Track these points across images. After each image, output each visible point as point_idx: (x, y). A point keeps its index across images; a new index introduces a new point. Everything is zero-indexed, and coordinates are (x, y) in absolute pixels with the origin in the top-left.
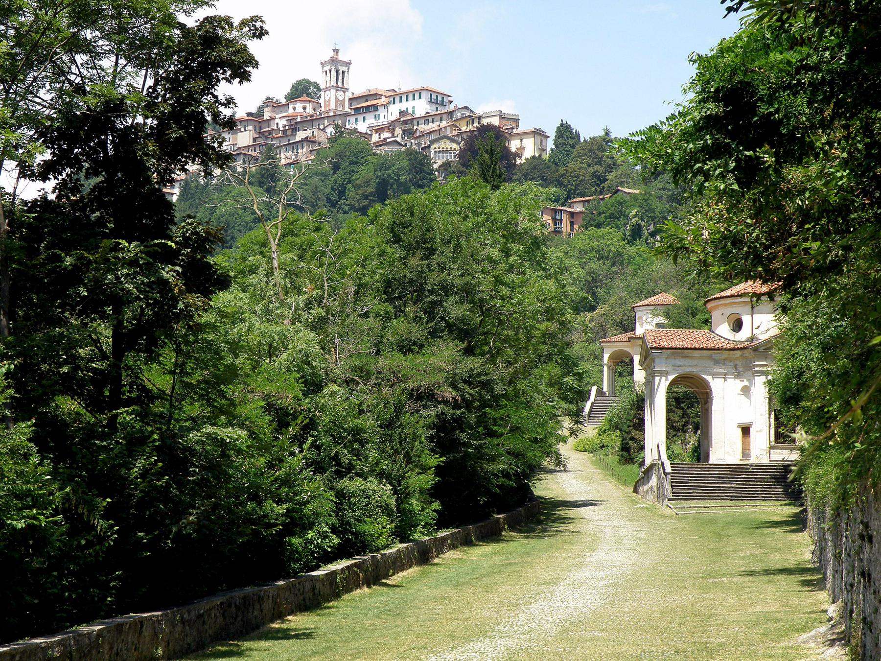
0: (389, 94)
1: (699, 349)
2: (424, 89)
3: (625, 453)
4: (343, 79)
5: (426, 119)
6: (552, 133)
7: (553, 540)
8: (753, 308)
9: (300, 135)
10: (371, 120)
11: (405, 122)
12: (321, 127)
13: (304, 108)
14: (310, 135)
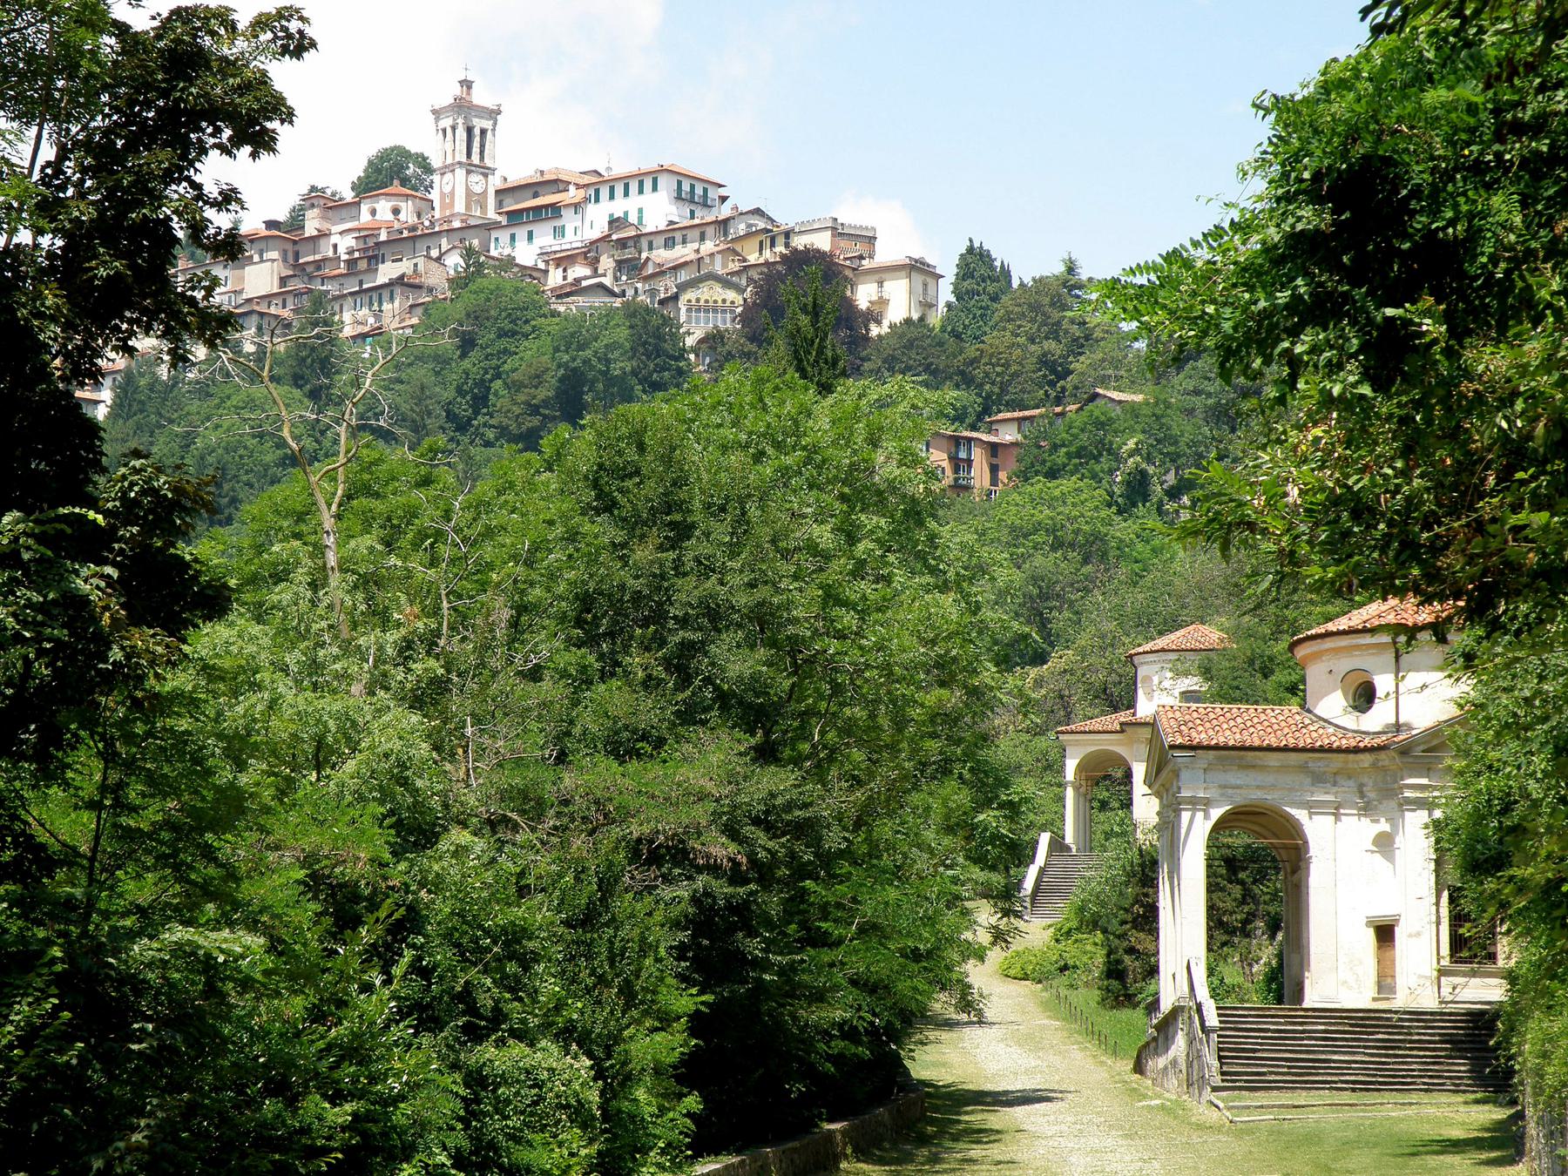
0: (587, 180)
2: (663, 170)
3: (1115, 983)
4: (482, 146)
5: (670, 235)
6: (948, 269)
8: (1397, 658)
9: (387, 272)
10: (544, 238)
11: (622, 244)
12: (434, 253)
13: (396, 211)
14: (410, 272)
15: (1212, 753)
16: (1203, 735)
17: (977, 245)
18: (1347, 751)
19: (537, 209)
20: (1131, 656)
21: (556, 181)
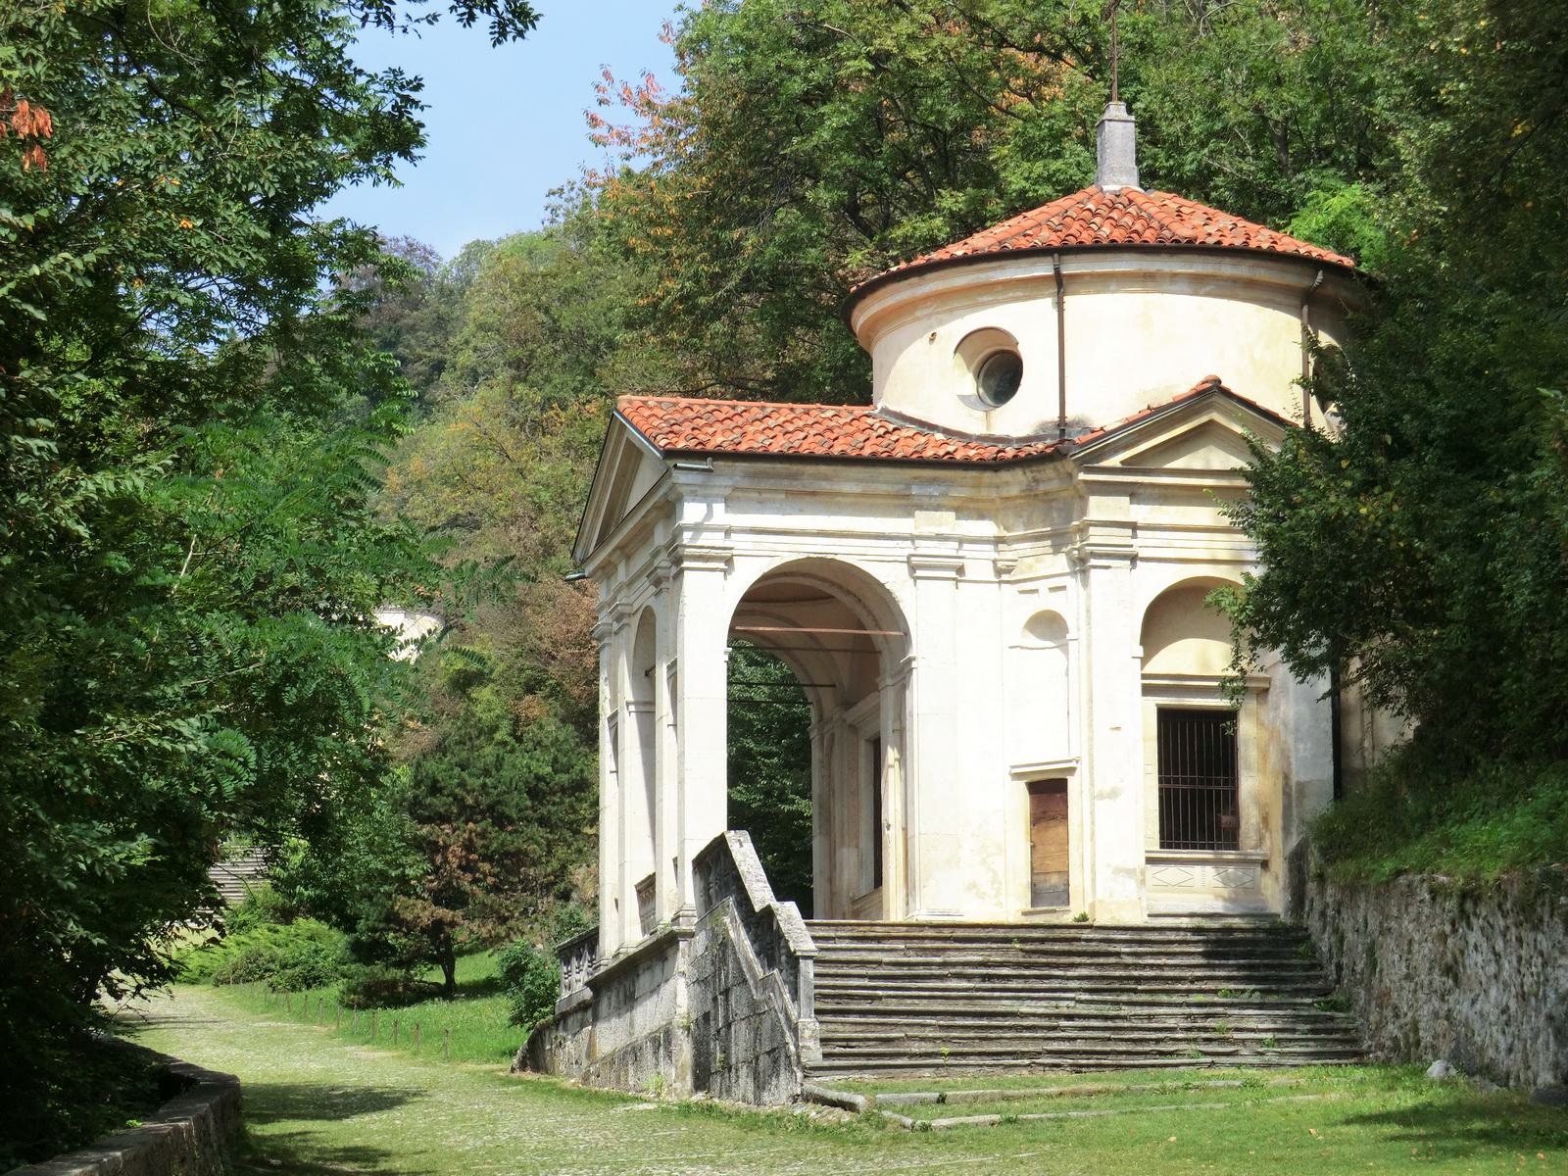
15: (742, 466)
18: (981, 465)
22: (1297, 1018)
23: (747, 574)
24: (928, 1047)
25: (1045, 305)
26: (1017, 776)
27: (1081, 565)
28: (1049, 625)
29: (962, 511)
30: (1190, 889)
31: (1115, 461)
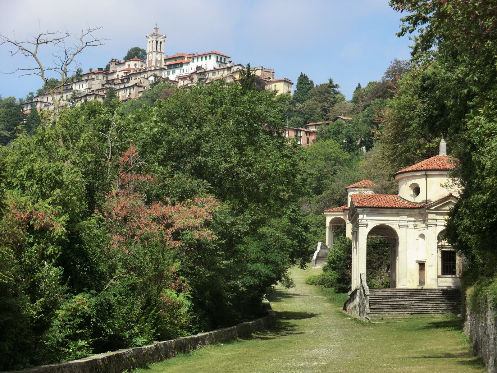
0: (191, 56)
1: (389, 208)
2: (213, 53)
4: (160, 46)
5: (214, 71)
6: (295, 81)
7: (288, 337)
9: (132, 82)
10: (178, 72)
11: (200, 73)
12: (146, 77)
13: (135, 65)
14: (139, 82)
15: (369, 209)
16: (366, 204)
17: (303, 74)
18: (411, 208)
19: (176, 64)
20: (346, 189)
21: (182, 57)
22: (452, 306)
23: (370, 227)
24: (388, 310)
25: (424, 179)
26: (417, 262)
27: (427, 226)
28: (422, 236)
29: (408, 216)
30: (446, 282)
31: (433, 208)
